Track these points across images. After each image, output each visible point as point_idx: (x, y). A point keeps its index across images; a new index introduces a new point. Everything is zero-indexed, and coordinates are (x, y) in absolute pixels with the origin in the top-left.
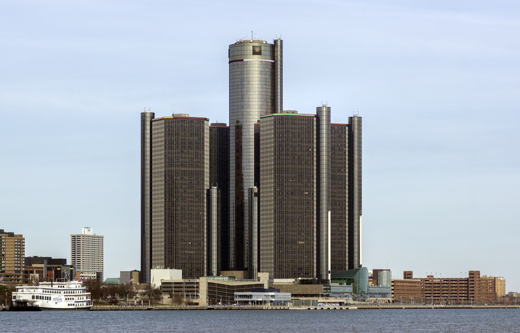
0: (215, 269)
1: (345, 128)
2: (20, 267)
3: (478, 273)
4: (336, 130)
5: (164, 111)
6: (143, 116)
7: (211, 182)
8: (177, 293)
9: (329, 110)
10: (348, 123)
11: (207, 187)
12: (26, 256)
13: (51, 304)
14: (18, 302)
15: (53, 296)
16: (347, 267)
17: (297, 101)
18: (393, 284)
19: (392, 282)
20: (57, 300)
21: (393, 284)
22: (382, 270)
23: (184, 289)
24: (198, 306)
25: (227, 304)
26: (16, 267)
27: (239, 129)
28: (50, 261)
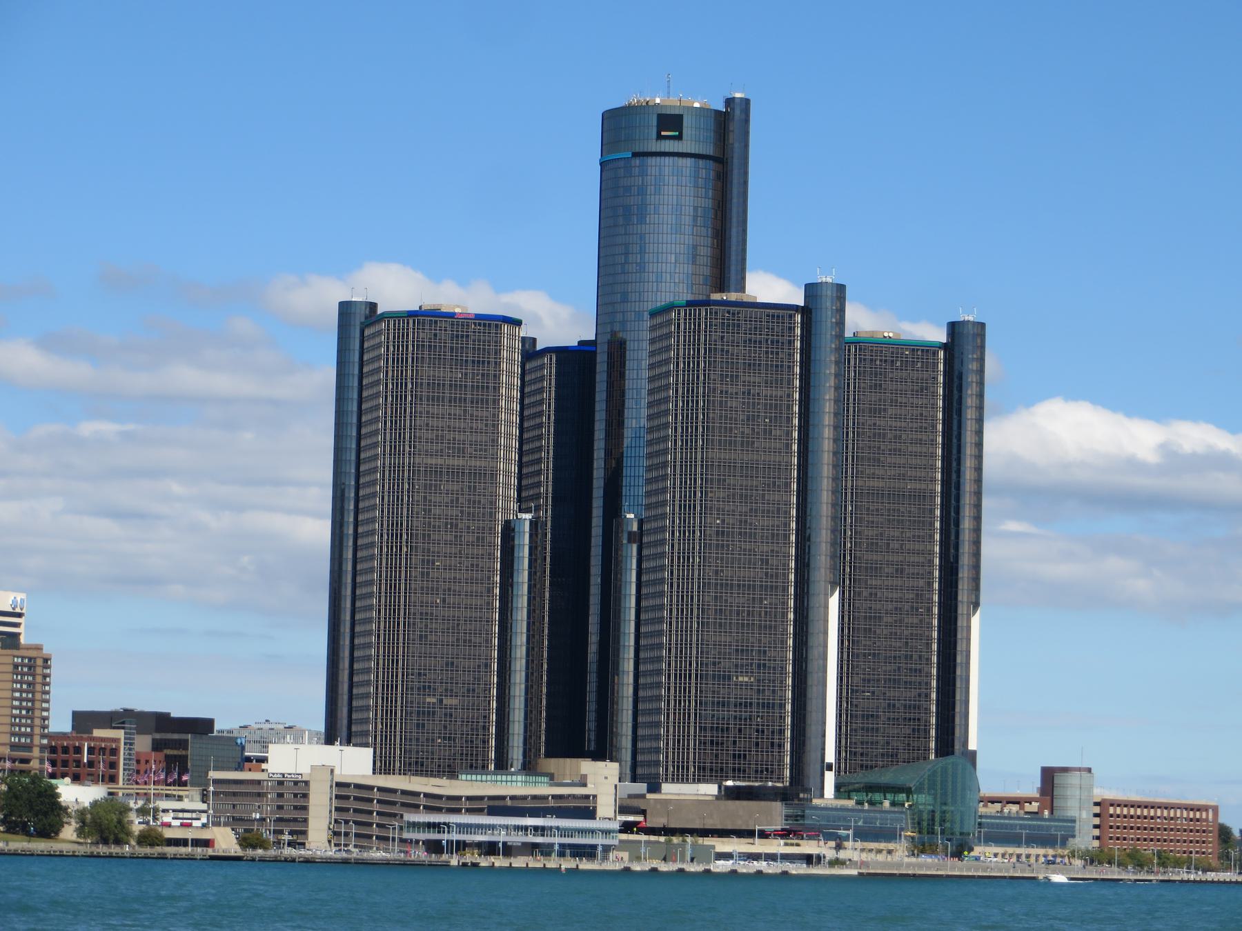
0: (516, 753)
1: (935, 354)
2: (31, 735)
8: (385, 821)
10: (944, 340)
18: (1097, 810)
19: (1096, 804)
21: (1097, 810)
22: (1065, 770)
23: (376, 807)
24: (302, 852)
25: (1150, 872)
26: (13, 734)
27: (618, 350)
28: (162, 721)
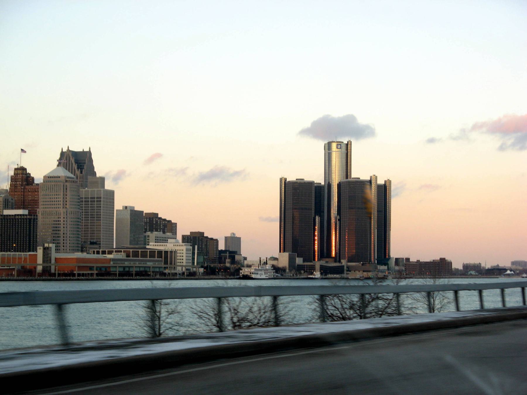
3: (203, 233)
4: (379, 187)
5: (291, 178)
6: (281, 179)
7: (315, 213)
9: (376, 177)
11: (313, 216)
12: (220, 249)
13: (258, 276)
14: (243, 275)
15: (259, 272)
16: (383, 256)
17: (359, 172)
20: (261, 274)
27: (329, 186)
